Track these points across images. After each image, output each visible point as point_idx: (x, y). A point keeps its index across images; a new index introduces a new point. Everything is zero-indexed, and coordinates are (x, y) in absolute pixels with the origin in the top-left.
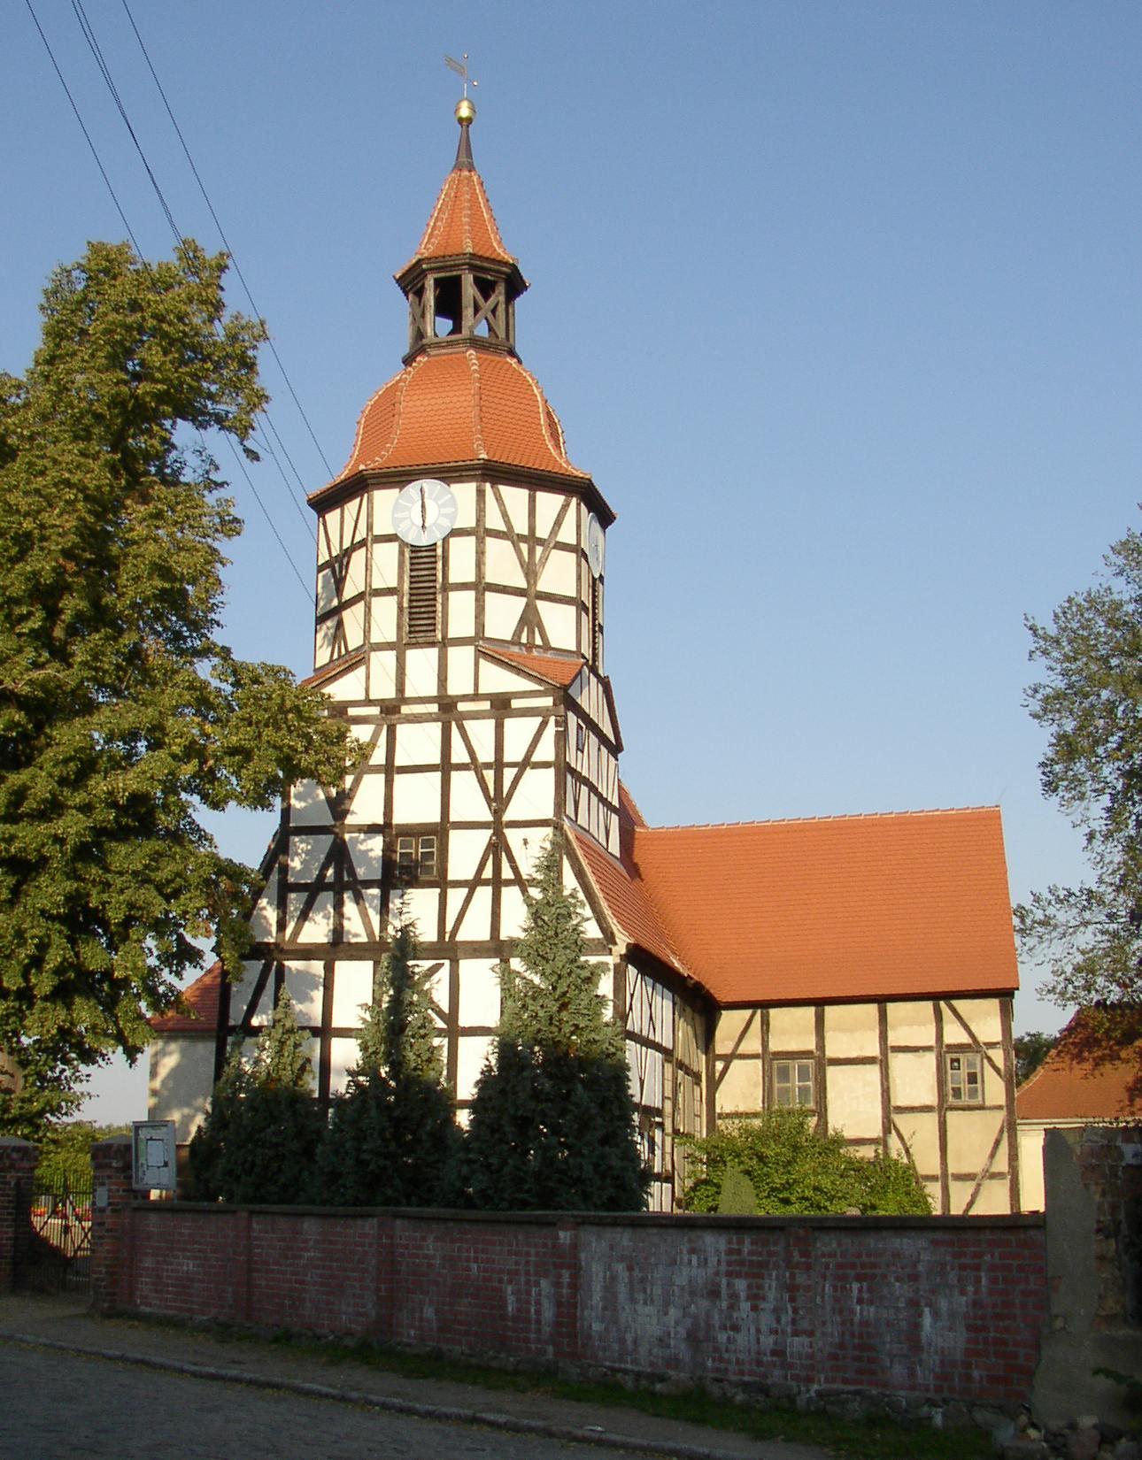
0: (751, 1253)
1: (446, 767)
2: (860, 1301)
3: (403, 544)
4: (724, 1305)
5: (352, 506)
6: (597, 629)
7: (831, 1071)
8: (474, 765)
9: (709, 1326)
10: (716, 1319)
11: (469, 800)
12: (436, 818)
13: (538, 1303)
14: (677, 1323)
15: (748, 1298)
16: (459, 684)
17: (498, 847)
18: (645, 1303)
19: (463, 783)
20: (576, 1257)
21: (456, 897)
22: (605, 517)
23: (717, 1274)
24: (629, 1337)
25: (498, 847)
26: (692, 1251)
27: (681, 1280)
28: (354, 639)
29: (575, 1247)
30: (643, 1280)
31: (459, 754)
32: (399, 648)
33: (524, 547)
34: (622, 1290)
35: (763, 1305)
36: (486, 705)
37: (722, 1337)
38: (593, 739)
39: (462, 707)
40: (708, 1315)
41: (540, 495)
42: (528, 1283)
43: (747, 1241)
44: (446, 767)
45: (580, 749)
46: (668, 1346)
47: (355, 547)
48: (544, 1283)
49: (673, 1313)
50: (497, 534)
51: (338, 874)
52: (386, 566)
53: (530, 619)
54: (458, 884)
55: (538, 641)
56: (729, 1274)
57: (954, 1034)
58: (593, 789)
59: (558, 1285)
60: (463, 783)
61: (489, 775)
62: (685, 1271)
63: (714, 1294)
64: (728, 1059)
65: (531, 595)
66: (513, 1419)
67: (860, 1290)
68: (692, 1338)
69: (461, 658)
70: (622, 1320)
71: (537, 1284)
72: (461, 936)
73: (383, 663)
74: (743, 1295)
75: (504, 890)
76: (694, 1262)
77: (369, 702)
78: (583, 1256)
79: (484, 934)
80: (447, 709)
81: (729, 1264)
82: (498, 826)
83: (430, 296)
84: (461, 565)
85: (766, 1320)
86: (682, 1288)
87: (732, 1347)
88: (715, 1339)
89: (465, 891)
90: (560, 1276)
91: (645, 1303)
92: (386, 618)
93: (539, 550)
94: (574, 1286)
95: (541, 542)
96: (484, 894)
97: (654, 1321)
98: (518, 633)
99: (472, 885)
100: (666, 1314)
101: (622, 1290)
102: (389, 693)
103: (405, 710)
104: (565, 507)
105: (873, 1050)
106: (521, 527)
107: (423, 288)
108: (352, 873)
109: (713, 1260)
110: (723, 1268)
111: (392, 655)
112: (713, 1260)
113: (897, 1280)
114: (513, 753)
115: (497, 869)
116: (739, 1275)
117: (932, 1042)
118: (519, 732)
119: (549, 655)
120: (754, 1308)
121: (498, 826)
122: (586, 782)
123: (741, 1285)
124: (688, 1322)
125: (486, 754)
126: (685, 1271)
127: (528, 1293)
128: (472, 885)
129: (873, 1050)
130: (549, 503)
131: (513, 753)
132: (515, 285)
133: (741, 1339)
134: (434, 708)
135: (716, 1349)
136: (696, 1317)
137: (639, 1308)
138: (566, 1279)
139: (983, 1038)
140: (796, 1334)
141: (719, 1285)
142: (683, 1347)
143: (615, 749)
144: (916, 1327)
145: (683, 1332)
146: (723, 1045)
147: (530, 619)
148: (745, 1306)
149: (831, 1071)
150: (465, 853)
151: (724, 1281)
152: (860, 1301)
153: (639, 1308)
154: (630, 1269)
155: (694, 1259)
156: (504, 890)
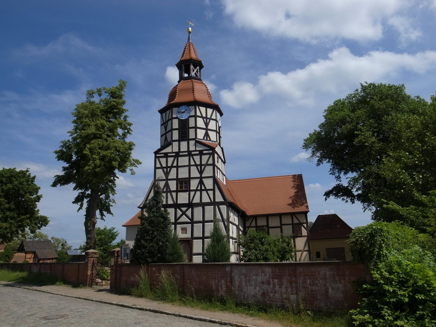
0: (278, 273)
1: (189, 166)
2: (310, 285)
3: (179, 119)
4: (272, 286)
5: (168, 112)
6: (220, 137)
7: (270, 229)
8: (196, 165)
9: (268, 292)
10: (270, 291)
11: (195, 173)
12: (179, 193)
13: (221, 286)
14: (259, 291)
15: (278, 284)
16: (192, 148)
17: (201, 183)
18: (250, 286)
19: (193, 169)
20: (231, 274)
21: (192, 193)
22: (221, 114)
23: (269, 278)
24: (246, 295)
25: (201, 183)
26: (262, 272)
27: (259, 280)
28: (169, 140)
29: (231, 272)
30: (249, 280)
31: (192, 163)
32: (179, 141)
33: (205, 119)
34: (244, 283)
35: (282, 286)
36: (198, 153)
37: (271, 295)
38: (220, 160)
39: (193, 153)
40: (267, 289)
41: (208, 109)
42: (218, 281)
43: (277, 269)
44: (189, 166)
45: (218, 162)
46: (256, 297)
47: (169, 120)
48: (223, 281)
49: (258, 288)
50: (199, 117)
51: (167, 190)
52: (176, 124)
53: (207, 135)
54: (193, 190)
55: (208, 139)
56: (272, 278)
57: (296, 221)
58: (220, 170)
59: (226, 282)
60: (193, 169)
61: (199, 167)
62: (260, 277)
63: (269, 283)
64: (248, 227)
65: (207, 129)
66: (220, 321)
67: (310, 282)
68: (263, 294)
69: (192, 143)
70: (244, 290)
71: (221, 282)
72: (194, 202)
73: (175, 144)
74: (277, 284)
75: (203, 192)
76: (263, 274)
77: (172, 153)
78: (233, 274)
79: (198, 201)
80: (190, 154)
81: (272, 275)
82: (201, 178)
83: (183, 68)
84: (192, 123)
85: (283, 290)
86: (260, 282)
87: (274, 298)
88: (269, 295)
89: (194, 192)
90: (227, 279)
91: (250, 286)
92: (176, 135)
93: (208, 120)
94: (231, 282)
95: (208, 118)
96: (198, 193)
97: (253, 290)
98: (204, 138)
99: (196, 191)
100: (256, 289)
101: (244, 283)
102: (177, 150)
103: (169, 194)
104: (213, 112)
105: (279, 225)
106: (204, 115)
107: (182, 67)
108: (170, 189)
109: (268, 275)
110: (271, 276)
111: (177, 142)
112: (268, 275)
113: (320, 279)
114: (204, 162)
115: (201, 187)
116: (275, 278)
117: (291, 223)
118: (205, 158)
119: (210, 142)
120: (280, 287)
121: (201, 178)
122: (219, 169)
123: (276, 281)
124: (262, 291)
125: (198, 163)
126: (260, 277)
127: (218, 284)
128: (196, 191)
129: (279, 225)
130: (210, 111)
131: (204, 162)
132: (201, 67)
133: (277, 295)
134: (187, 153)
135: (270, 298)
136: (264, 290)
137: (248, 287)
138: (229, 279)
139: (302, 222)
140: (292, 294)
141: (270, 281)
142: (261, 297)
143: (224, 163)
144: (327, 291)
145: (260, 293)
146: (248, 225)
147: (207, 135)
148: (277, 287)
149: (270, 229)
150: (194, 184)
151: (271, 280)
152: (310, 285)
153: (248, 287)
154: (245, 277)
155: (263, 274)
156: (203, 192)
